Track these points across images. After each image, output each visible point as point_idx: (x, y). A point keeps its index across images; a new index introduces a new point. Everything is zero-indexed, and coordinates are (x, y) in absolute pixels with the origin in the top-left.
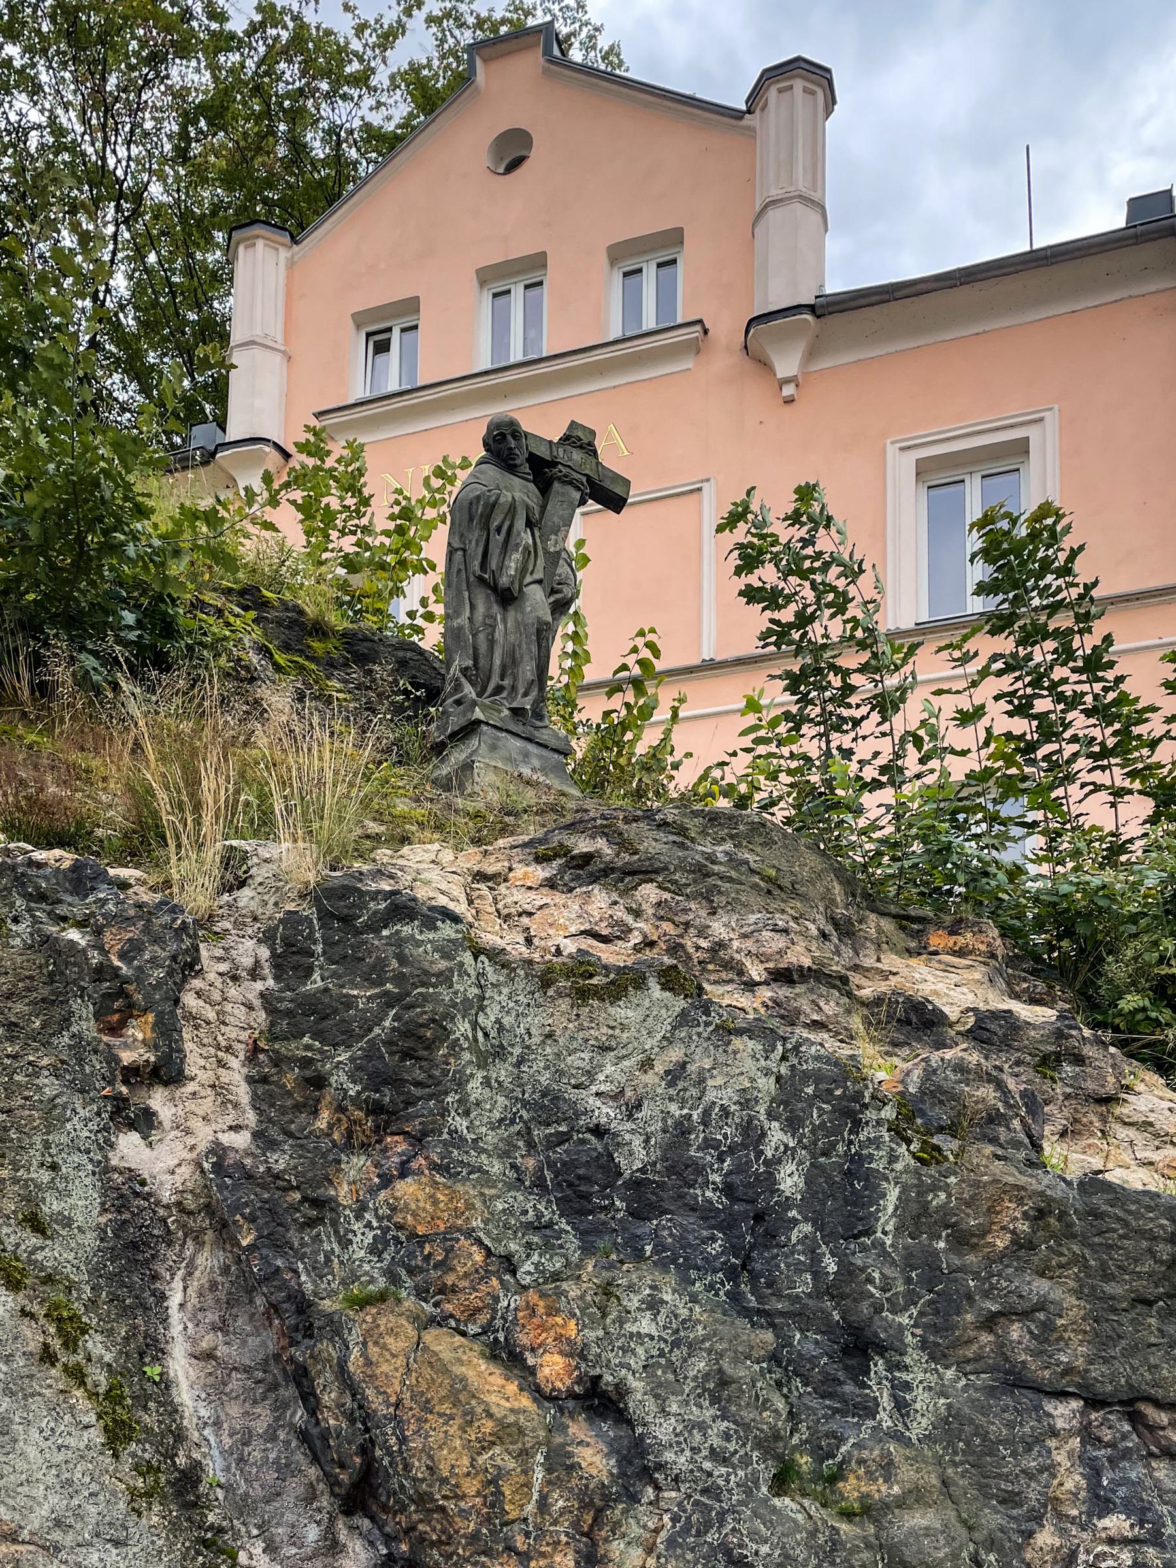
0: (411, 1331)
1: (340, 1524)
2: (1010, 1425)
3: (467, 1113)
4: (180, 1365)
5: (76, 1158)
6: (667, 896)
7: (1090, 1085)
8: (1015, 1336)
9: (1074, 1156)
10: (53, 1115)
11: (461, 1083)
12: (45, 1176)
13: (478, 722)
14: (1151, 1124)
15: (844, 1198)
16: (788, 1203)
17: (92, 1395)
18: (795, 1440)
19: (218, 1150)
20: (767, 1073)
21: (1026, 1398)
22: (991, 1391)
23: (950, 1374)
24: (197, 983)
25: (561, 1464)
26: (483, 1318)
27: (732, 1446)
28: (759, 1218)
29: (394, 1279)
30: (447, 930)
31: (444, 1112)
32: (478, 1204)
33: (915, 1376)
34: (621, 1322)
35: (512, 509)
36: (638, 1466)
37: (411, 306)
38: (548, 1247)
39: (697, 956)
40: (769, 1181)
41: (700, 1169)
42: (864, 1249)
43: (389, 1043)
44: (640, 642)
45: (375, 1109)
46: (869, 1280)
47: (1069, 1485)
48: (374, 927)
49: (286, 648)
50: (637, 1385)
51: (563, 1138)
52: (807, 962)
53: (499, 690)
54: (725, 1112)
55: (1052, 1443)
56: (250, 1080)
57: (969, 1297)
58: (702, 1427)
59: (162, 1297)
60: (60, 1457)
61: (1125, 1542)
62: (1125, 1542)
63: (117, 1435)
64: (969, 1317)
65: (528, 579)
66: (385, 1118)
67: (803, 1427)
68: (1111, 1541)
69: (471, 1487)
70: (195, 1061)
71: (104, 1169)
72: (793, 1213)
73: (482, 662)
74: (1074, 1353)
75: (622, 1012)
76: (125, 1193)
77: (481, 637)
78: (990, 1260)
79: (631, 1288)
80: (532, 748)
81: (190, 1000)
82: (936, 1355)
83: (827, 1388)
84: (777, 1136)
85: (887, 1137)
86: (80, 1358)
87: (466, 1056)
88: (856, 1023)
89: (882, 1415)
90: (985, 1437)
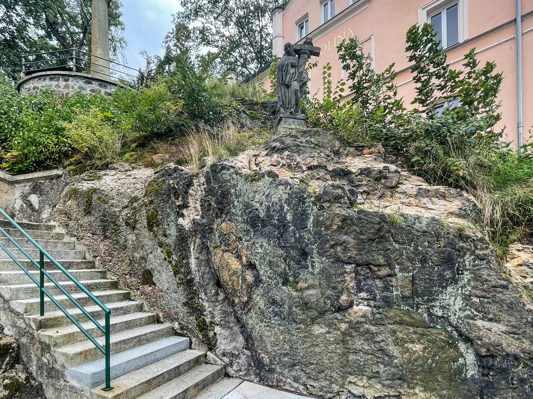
0: (221, 253)
1: (219, 290)
2: (336, 271)
3: (235, 208)
4: (193, 261)
5: (173, 223)
6: (289, 153)
7: (388, 184)
8: (338, 249)
9: (381, 203)
10: (168, 215)
11: (233, 203)
12: (167, 227)
13: (282, 117)
14: (406, 192)
15: (301, 219)
16: (289, 222)
17: (172, 266)
18: (290, 274)
19: (194, 220)
20: (285, 193)
21: (340, 264)
22: (333, 263)
23: (324, 259)
24: (192, 188)
25: (244, 280)
26: (236, 250)
27: (272, 275)
28: (284, 226)
29: (221, 243)
30: (232, 170)
31: (230, 208)
32: (234, 227)
33: (316, 259)
34: (254, 250)
35: (287, 65)
36: (258, 280)
37: (306, 15)
38: (247, 234)
39: (293, 166)
40: (285, 217)
41: (273, 216)
42: (306, 231)
43: (220, 196)
44: (339, 84)
45: (219, 209)
46: (305, 238)
47: (351, 285)
48: (219, 172)
49: (249, 109)
50: (257, 263)
51: (251, 212)
52: (316, 164)
53: (288, 108)
54: (276, 203)
55: (346, 275)
56: (201, 206)
57: (328, 241)
58: (267, 271)
59: (189, 248)
60: (167, 277)
61: (366, 299)
62: (366, 299)
63: (176, 273)
64: (328, 246)
65: (293, 80)
66: (221, 210)
67: (291, 271)
68: (362, 299)
69: (230, 283)
70: (191, 204)
71: (177, 225)
72: (290, 224)
73: (285, 103)
74: (353, 253)
75: (260, 183)
76: (180, 229)
77: (284, 97)
78: (332, 232)
79: (257, 243)
80: (295, 120)
81: (191, 191)
82: (321, 255)
83: (298, 262)
84: (286, 207)
85: (311, 205)
86: (171, 259)
87: (234, 196)
88: (328, 177)
89: (310, 268)
90: (330, 274)
